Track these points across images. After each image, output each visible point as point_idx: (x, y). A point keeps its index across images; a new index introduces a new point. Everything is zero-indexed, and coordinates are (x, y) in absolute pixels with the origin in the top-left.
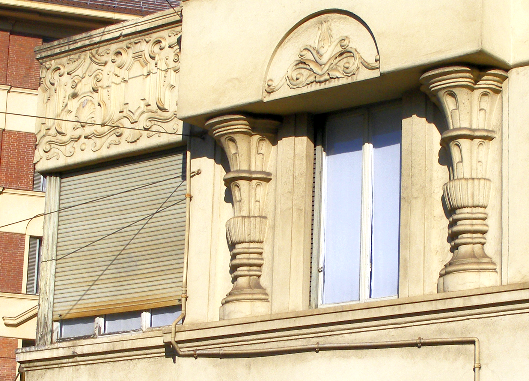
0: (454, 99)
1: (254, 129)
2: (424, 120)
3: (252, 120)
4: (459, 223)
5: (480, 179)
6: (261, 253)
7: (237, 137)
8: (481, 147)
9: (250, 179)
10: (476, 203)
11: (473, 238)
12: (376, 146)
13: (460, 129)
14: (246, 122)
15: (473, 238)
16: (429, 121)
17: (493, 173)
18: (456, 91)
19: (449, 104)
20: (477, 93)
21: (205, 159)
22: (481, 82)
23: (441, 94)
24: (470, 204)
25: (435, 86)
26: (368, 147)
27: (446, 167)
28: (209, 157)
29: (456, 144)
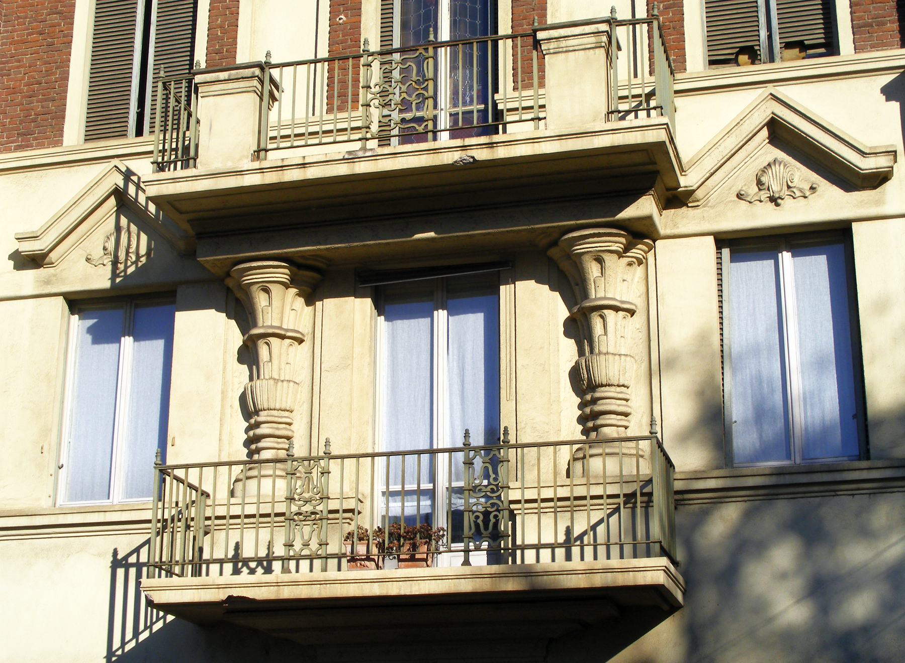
0: (599, 266)
1: (294, 282)
2: (546, 287)
3: (295, 269)
4: (263, 426)
5: (615, 355)
6: (290, 424)
7: (607, 257)
8: (291, 348)
9: (282, 337)
10: (283, 407)
11: (278, 443)
12: (136, 339)
13: (605, 298)
14: (287, 271)
15: (278, 443)
16: (552, 289)
17: (303, 376)
18: (271, 286)
19: (261, 300)
20: (625, 261)
21: (212, 312)
22: (634, 250)
23: (254, 288)
24: (278, 407)
25: (579, 248)
26: (127, 342)
27: (245, 368)
28: (219, 310)
29: (266, 343)
